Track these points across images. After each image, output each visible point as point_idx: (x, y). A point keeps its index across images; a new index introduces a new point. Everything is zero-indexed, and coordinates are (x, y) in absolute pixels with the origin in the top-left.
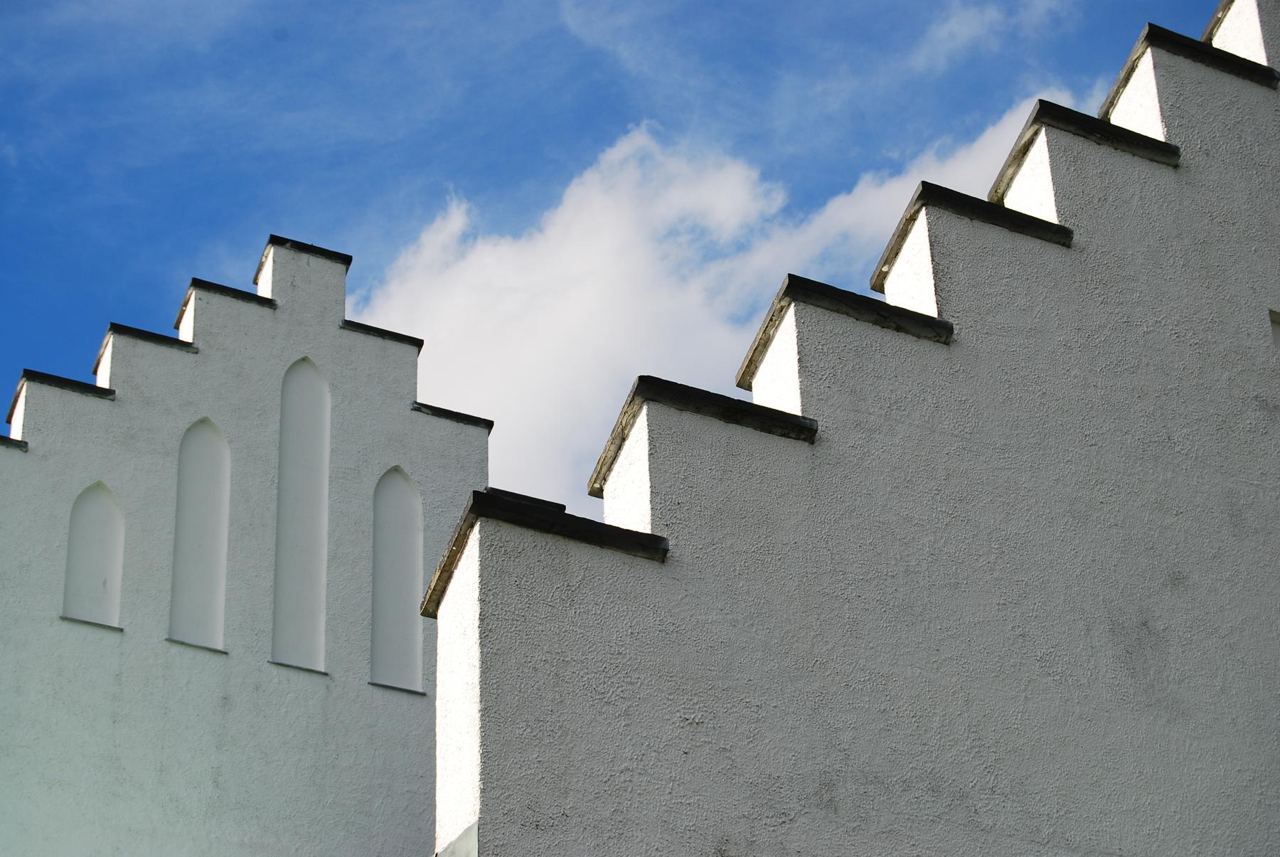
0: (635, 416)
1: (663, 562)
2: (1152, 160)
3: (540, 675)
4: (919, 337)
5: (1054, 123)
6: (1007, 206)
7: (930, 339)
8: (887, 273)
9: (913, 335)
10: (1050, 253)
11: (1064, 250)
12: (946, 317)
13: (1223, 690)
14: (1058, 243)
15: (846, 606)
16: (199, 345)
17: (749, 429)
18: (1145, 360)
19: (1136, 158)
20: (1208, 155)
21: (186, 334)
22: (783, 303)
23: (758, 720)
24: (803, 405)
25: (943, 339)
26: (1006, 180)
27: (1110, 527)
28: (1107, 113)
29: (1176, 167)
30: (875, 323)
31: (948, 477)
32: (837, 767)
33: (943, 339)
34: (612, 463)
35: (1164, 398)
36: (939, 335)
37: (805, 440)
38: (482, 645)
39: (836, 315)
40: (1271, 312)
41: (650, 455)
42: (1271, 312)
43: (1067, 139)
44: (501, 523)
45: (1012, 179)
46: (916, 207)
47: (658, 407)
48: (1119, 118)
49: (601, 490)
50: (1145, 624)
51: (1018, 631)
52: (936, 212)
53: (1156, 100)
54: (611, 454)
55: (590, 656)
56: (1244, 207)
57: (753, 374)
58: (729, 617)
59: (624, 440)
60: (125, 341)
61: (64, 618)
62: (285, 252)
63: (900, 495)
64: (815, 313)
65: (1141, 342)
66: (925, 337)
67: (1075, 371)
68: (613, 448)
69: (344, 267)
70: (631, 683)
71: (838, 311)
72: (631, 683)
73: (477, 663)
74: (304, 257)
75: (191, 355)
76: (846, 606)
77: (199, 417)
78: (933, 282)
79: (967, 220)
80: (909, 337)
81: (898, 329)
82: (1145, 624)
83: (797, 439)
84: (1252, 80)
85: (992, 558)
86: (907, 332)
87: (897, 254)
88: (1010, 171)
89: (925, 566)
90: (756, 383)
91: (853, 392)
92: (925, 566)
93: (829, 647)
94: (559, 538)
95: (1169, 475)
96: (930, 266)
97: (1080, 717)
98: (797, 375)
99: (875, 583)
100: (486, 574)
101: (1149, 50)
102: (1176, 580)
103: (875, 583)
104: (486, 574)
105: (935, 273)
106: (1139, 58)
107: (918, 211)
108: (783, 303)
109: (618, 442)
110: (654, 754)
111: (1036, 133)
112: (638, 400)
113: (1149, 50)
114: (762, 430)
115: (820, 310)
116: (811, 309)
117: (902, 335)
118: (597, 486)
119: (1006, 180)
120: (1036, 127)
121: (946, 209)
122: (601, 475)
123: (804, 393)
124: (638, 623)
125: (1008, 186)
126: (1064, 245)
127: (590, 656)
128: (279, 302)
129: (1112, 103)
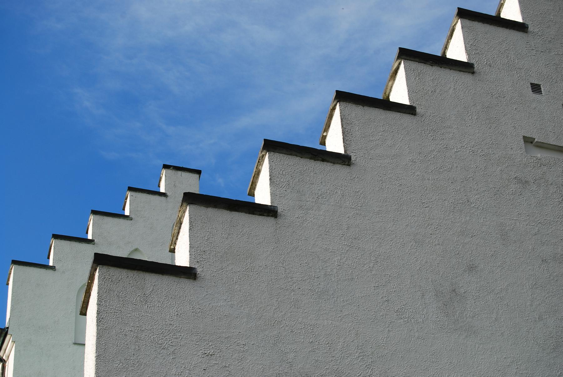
0: (184, 212)
1: (195, 279)
2: (460, 71)
3: (128, 338)
4: (334, 163)
5: (408, 58)
6: (391, 100)
7: (340, 164)
8: (326, 136)
9: (331, 162)
10: (406, 119)
11: (413, 117)
12: (348, 153)
13: (496, 319)
14: (409, 114)
15: (292, 294)
16: (133, 216)
17: (243, 214)
18: (455, 165)
19: (452, 71)
20: (490, 66)
21: (127, 213)
22: (263, 153)
23: (244, 351)
24: (271, 200)
25: (347, 163)
26: (389, 88)
27: (435, 245)
28: (444, 53)
29: (473, 73)
30: (311, 159)
31: (348, 228)
32: (286, 371)
33: (347, 163)
34: (178, 236)
35: (465, 182)
36: (344, 161)
37: (272, 216)
38: (98, 325)
39: (290, 156)
40: (524, 137)
41: (190, 229)
42: (524, 137)
43: (415, 65)
44: (110, 267)
45: (392, 87)
46: (335, 103)
47: (193, 207)
48: (450, 55)
49: (174, 249)
50: (454, 291)
51: (385, 299)
52: (344, 104)
53: (463, 43)
54: (176, 231)
55: (155, 327)
56: (509, 89)
57: (254, 189)
58: (230, 303)
59: (181, 224)
60: (98, 217)
61: (75, 344)
62: (170, 171)
63: (323, 239)
64: (278, 156)
65: (454, 157)
66: (337, 163)
67: (418, 173)
68: (177, 228)
69: (198, 176)
70: (176, 338)
71: (291, 155)
72: (176, 338)
73: (95, 334)
74: (180, 173)
75: (129, 221)
76: (292, 294)
77: (134, 248)
78: (342, 137)
79: (361, 107)
80: (329, 164)
81: (323, 160)
82: (454, 291)
83: (268, 216)
84: (514, 29)
85: (371, 265)
86: (328, 162)
87: (329, 126)
88: (390, 83)
89: (335, 271)
90: (256, 193)
91: (298, 192)
92: (335, 271)
93: (283, 314)
94: (141, 272)
95: (468, 218)
96: (341, 130)
97: (418, 338)
98: (269, 186)
99: (308, 281)
100: (101, 292)
101: (459, 20)
102: (472, 268)
103: (308, 281)
104: (101, 292)
105: (343, 133)
106: (455, 25)
107: (336, 105)
108: (263, 153)
109: (178, 225)
110: (187, 371)
111: (400, 64)
112: (185, 204)
113: (459, 20)
114: (250, 213)
115: (281, 155)
116: (277, 155)
117: (325, 163)
118: (172, 247)
119: (389, 88)
120: (399, 61)
121: (350, 102)
122: (173, 242)
123: (272, 194)
124: (181, 309)
125: (391, 90)
126: (412, 114)
127: (155, 327)
128: (168, 194)
129: (446, 48)
